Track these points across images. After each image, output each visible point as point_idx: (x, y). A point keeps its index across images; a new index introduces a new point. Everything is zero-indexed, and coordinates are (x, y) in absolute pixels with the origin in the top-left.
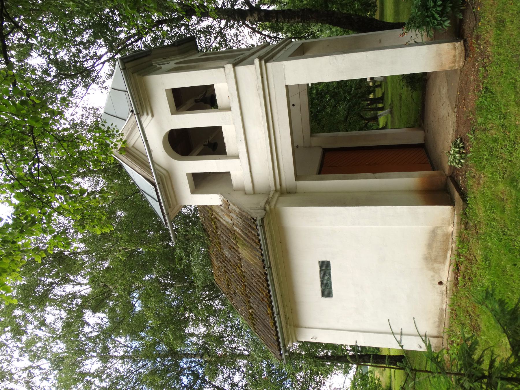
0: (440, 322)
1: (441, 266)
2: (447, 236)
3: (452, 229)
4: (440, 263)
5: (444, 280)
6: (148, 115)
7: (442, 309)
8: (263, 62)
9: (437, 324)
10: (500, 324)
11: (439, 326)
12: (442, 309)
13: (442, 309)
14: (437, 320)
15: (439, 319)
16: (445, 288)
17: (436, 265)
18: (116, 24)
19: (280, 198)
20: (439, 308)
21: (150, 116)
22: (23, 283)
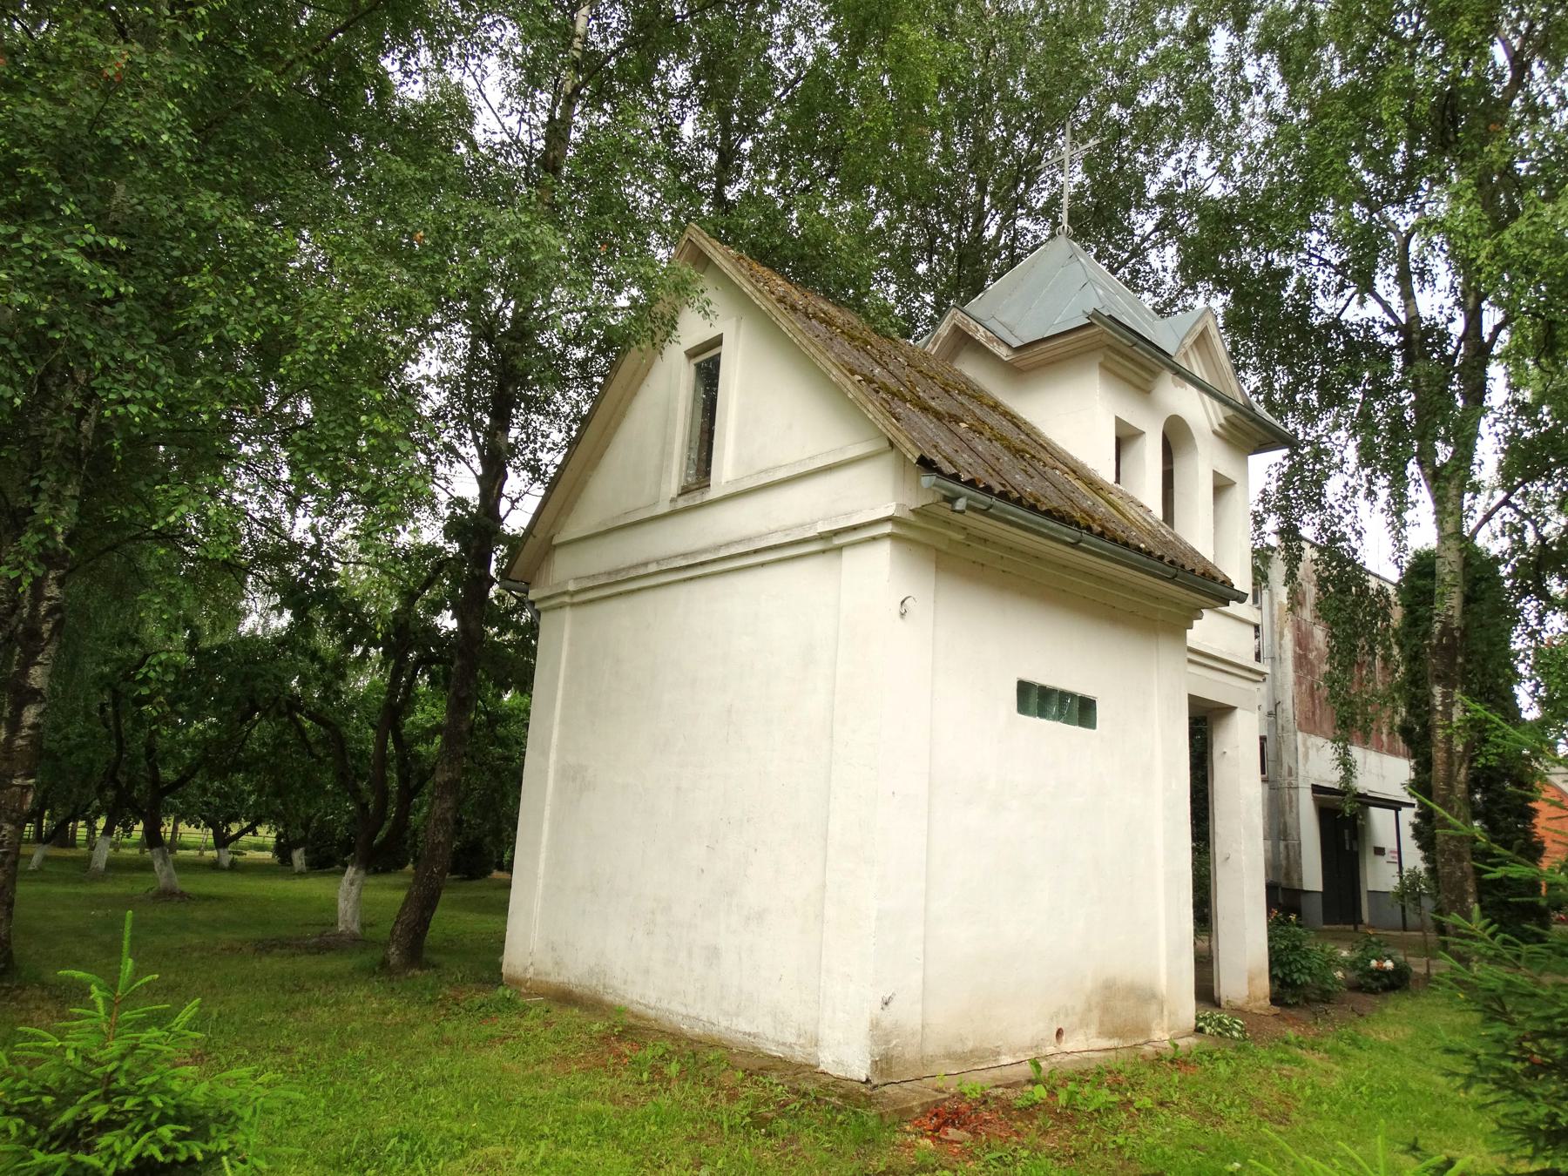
0: (961, 1058)
1: (1093, 1030)
2: (1144, 1030)
3: (1161, 1035)
4: (1102, 1023)
5: (1069, 1044)
6: (1220, 425)
7: (999, 1054)
8: (888, 528)
9: (958, 1048)
10: (1316, 1001)
11: (951, 1056)
12: (997, 1053)
13: (997, 1053)
14: (970, 1045)
15: (971, 1052)
16: (1050, 1050)
17: (1095, 1015)
18: (1394, 630)
19: (885, 548)
20: (1000, 1043)
21: (1217, 428)
22: (1474, 702)
